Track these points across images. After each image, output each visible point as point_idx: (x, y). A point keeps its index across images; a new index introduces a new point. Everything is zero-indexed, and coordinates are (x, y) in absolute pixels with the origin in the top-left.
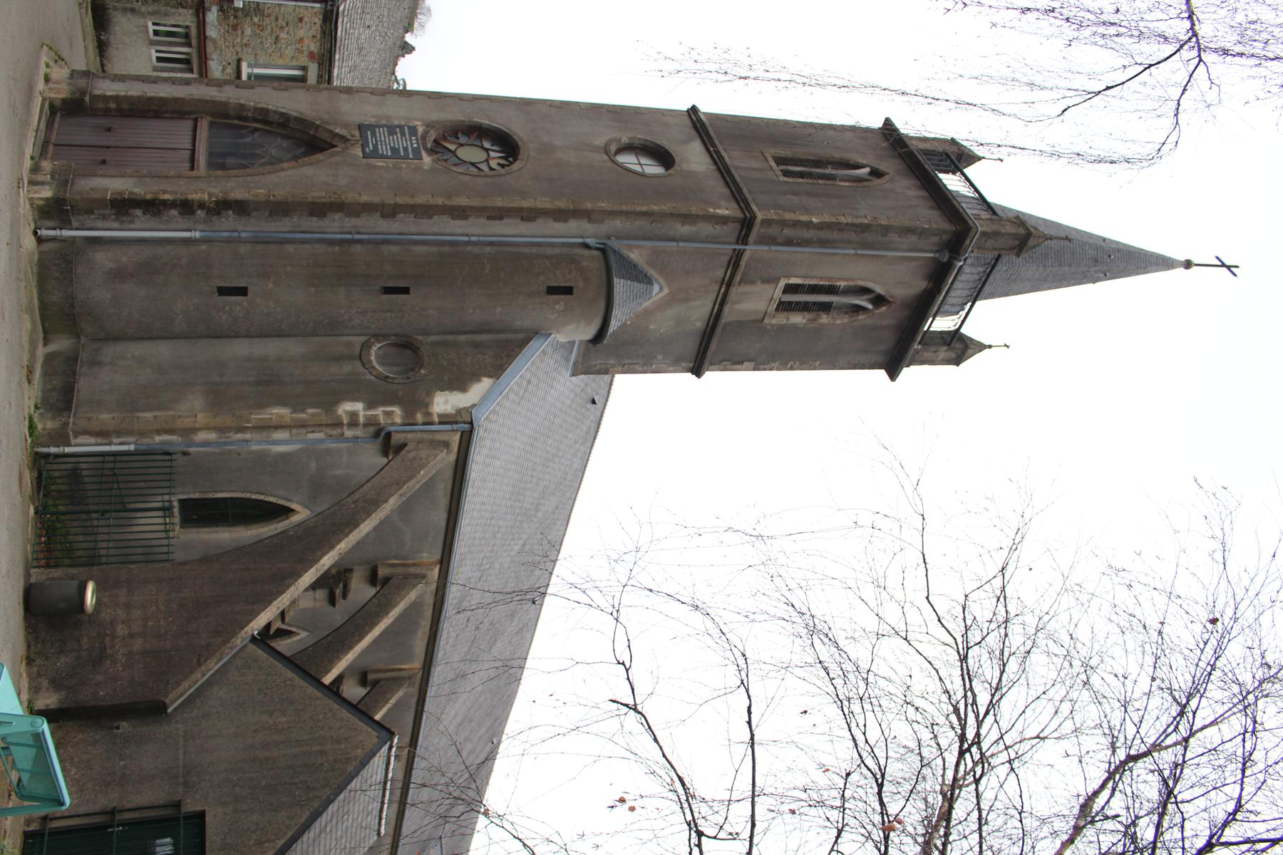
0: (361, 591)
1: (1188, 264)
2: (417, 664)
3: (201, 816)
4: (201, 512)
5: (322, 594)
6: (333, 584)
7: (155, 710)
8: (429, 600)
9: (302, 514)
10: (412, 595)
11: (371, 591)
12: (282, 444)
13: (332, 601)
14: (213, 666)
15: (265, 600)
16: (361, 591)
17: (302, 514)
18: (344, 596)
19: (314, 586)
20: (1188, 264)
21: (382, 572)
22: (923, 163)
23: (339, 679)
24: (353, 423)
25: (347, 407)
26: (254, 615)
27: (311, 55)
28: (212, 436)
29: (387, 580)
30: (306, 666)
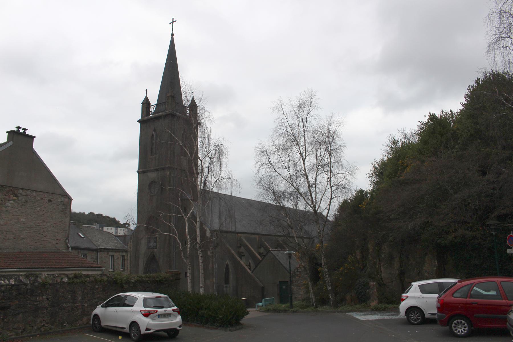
0: (242, 249)
1: (172, 35)
2: (257, 237)
3: (280, 282)
4: (227, 281)
5: (243, 258)
6: (241, 255)
7: (263, 288)
8: (245, 235)
9: (228, 262)
10: (244, 240)
11: (242, 248)
12: (216, 266)
13: (244, 256)
14: (256, 279)
15: (246, 270)
16: (242, 249)
17: (228, 262)
18: (243, 253)
19: (241, 259)
20: (172, 35)
21: (239, 245)
22: (143, 104)
23: (260, 254)
24: (213, 252)
25: (209, 253)
26: (248, 273)
27: (108, 254)
28: (214, 279)
29: (241, 245)
30: (257, 263)
